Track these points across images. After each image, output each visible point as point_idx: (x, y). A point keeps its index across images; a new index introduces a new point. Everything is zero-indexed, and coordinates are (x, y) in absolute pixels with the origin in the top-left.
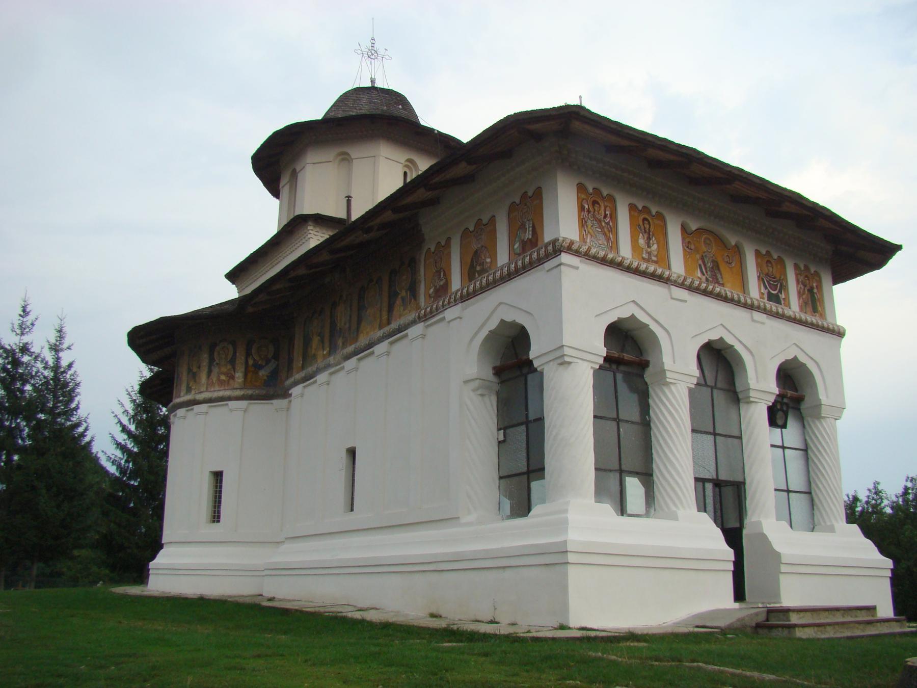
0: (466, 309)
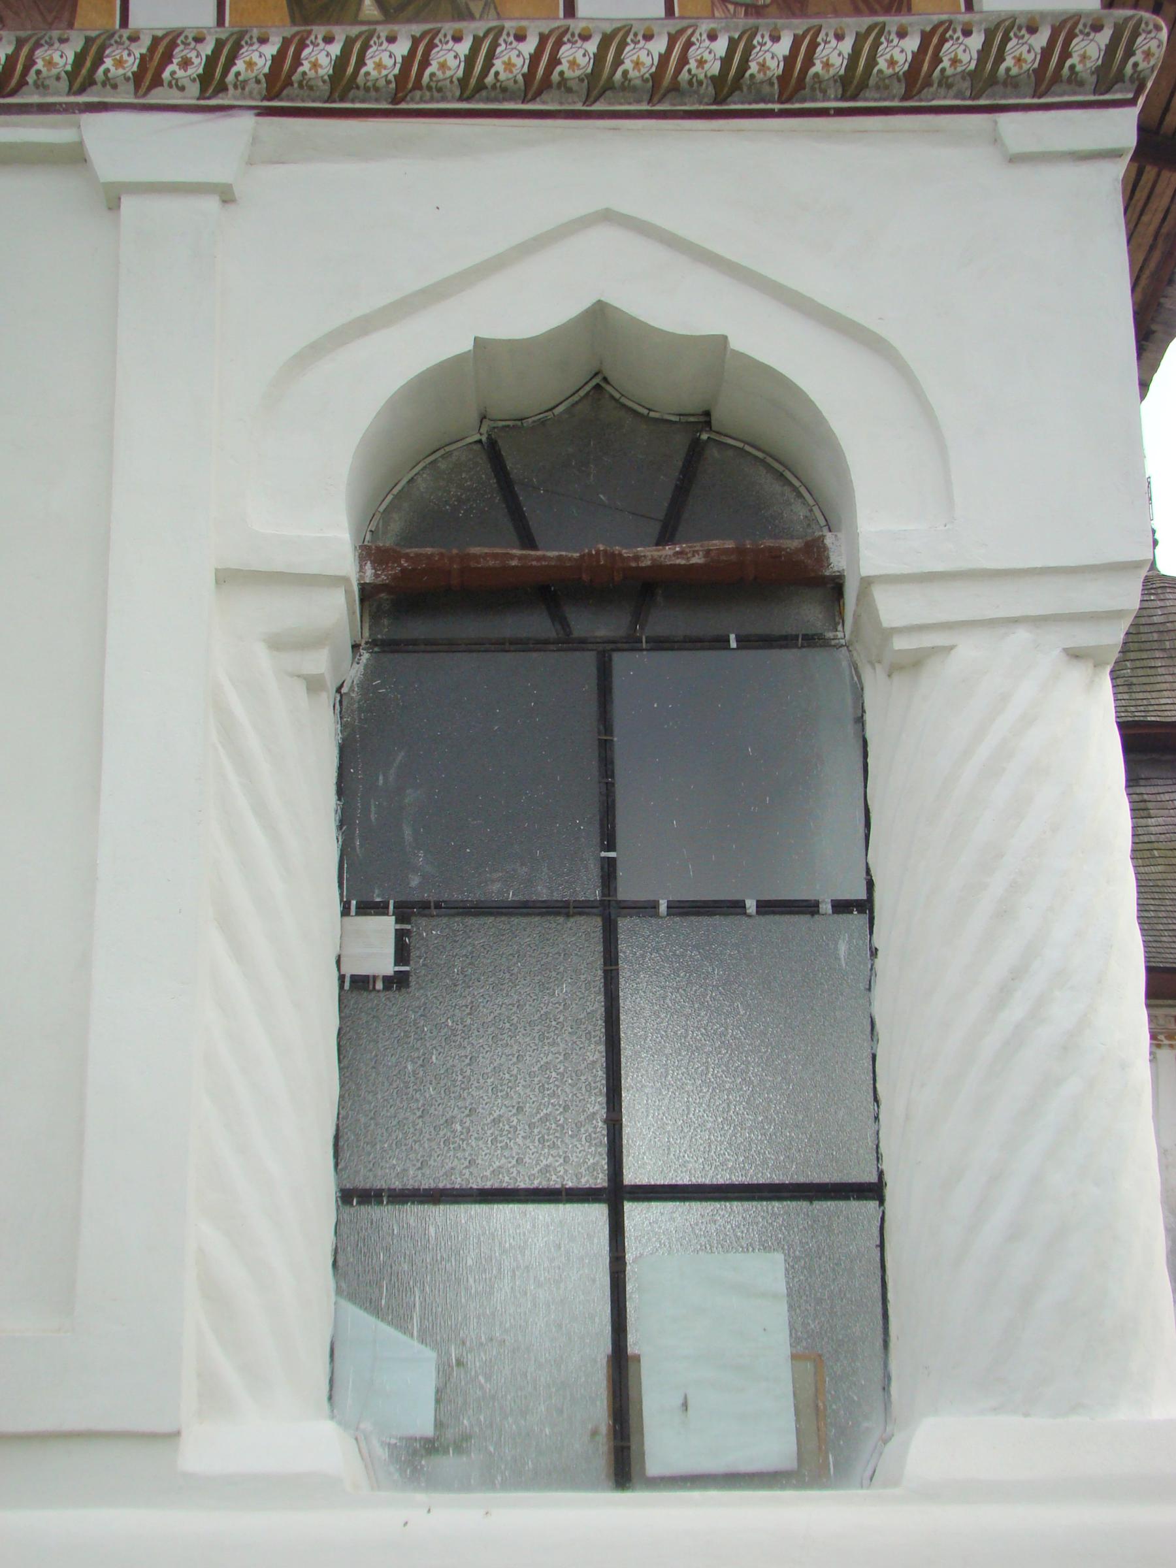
0: (278, 160)
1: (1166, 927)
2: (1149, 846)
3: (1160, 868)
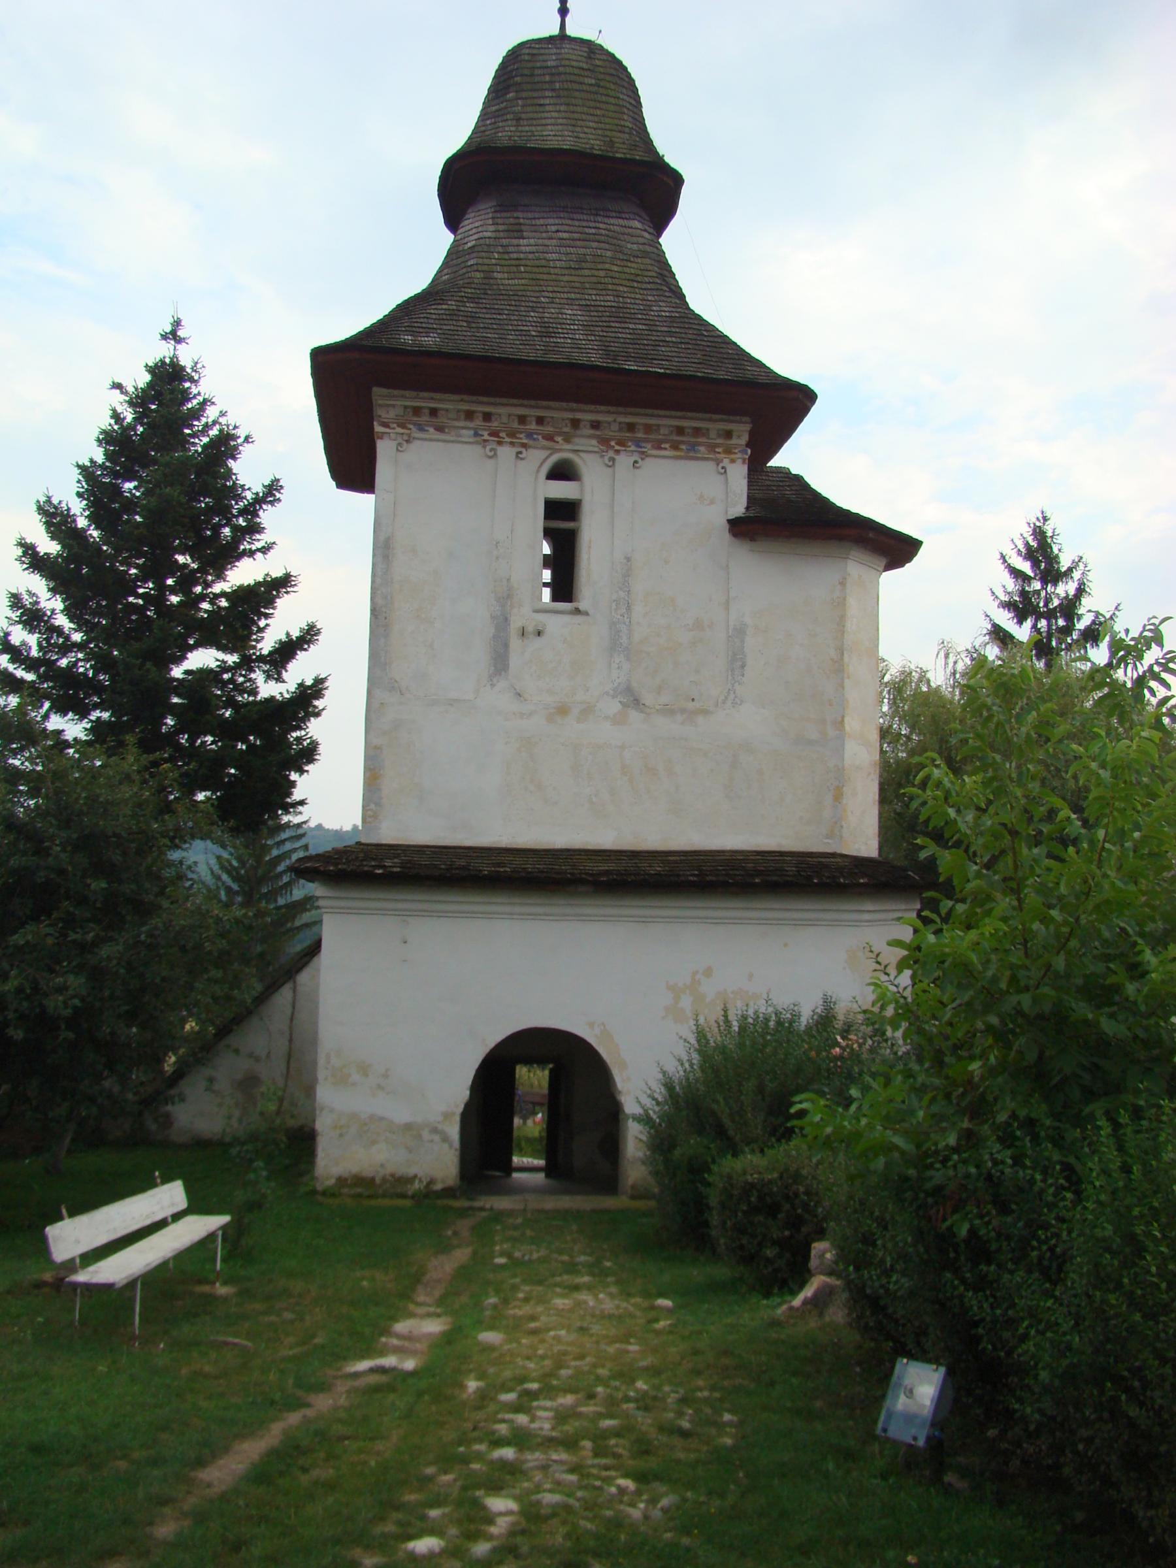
2: (517, 262)
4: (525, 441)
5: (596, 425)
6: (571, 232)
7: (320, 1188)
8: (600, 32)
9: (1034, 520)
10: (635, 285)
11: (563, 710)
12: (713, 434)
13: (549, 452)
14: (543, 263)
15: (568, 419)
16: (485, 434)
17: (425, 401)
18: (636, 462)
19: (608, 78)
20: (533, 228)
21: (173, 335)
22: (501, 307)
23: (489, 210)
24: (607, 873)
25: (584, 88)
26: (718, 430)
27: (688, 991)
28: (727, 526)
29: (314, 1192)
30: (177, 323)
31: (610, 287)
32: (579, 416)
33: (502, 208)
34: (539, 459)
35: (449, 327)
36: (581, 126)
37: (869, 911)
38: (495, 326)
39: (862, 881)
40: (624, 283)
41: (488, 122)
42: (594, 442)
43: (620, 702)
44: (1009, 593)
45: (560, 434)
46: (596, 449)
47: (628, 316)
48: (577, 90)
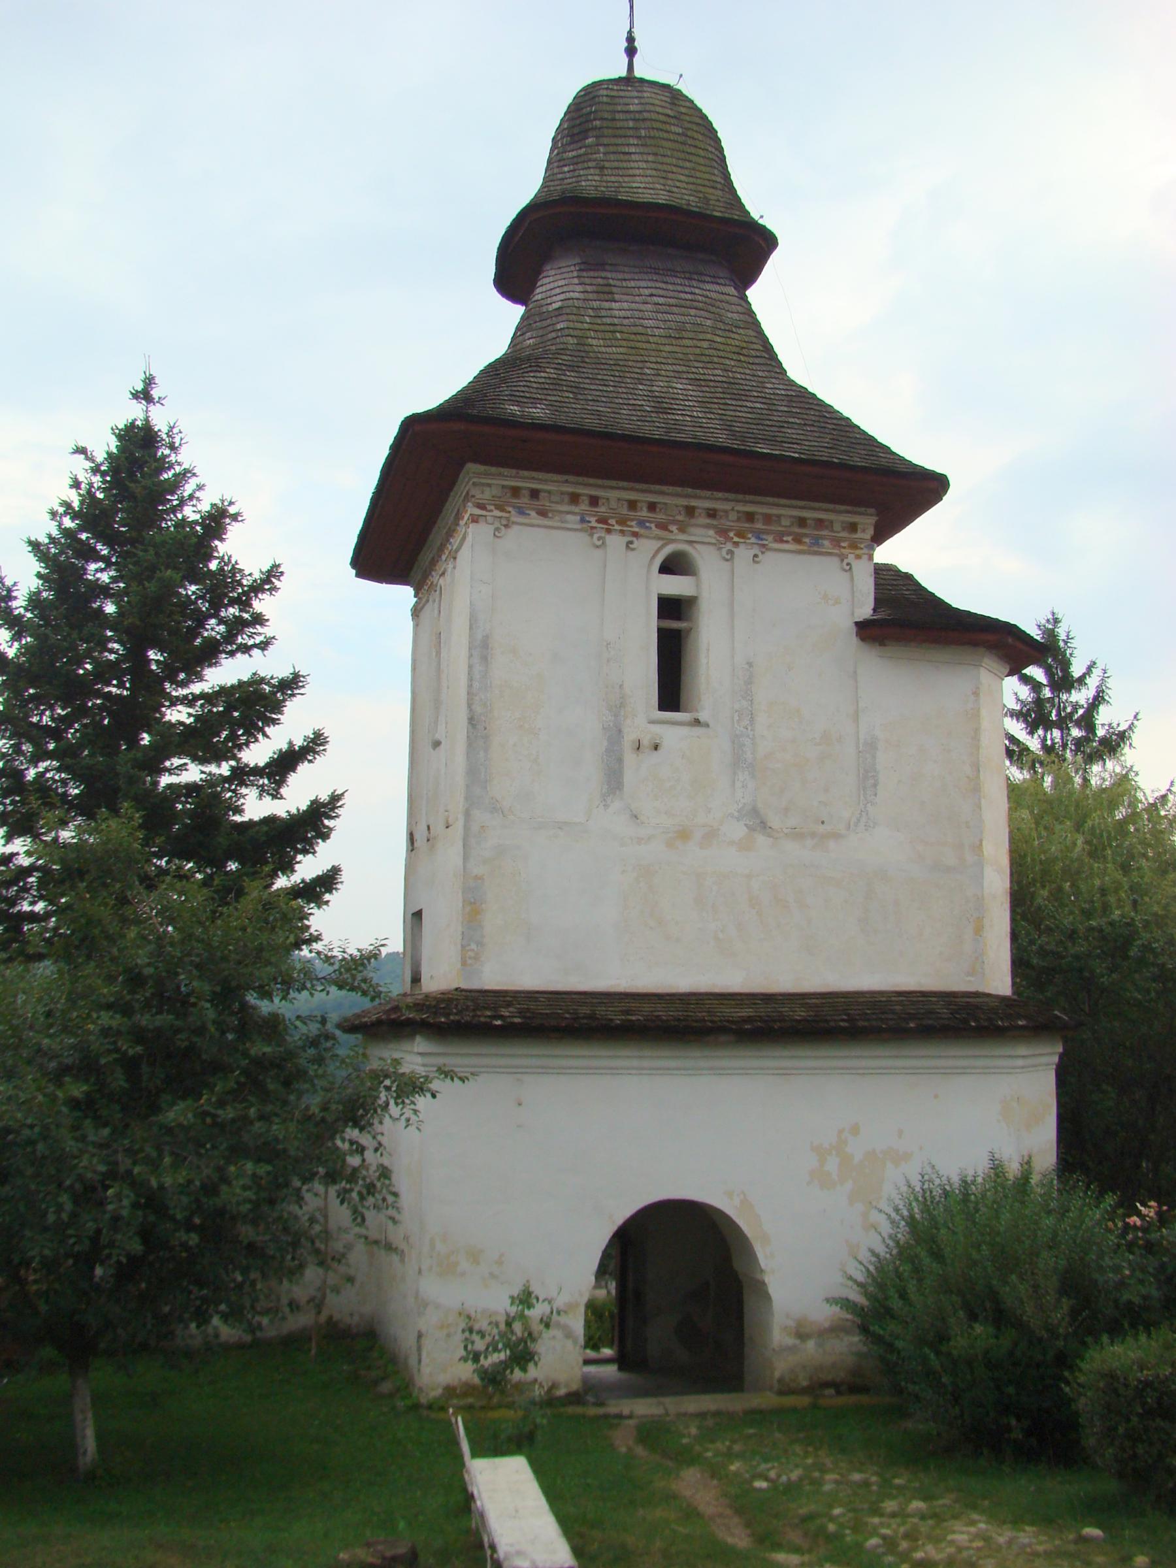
1: (626, 402)
2: (612, 328)
3: (621, 350)
4: (636, 530)
5: (712, 514)
6: (666, 297)
7: (423, 1400)
8: (681, 76)
9: (1043, 622)
10: (742, 358)
11: (684, 835)
12: (837, 527)
13: (660, 543)
14: (641, 330)
15: (682, 506)
16: (593, 519)
17: (526, 481)
18: (756, 556)
19: (695, 127)
20: (624, 290)
21: (145, 395)
22: (605, 378)
23: (572, 268)
24: (749, 1020)
25: (672, 137)
26: (843, 522)
27: (834, 1152)
28: (854, 630)
29: (416, 1406)
30: (149, 382)
31: (716, 360)
32: (694, 503)
33: (587, 266)
34: (651, 550)
35: (553, 398)
36: (672, 180)
37: (1023, 1057)
38: (604, 399)
39: (1020, 1023)
40: (730, 356)
41: (566, 169)
42: (711, 532)
43: (746, 825)
44: (1022, 702)
45: (674, 522)
46: (714, 541)
47: (743, 393)
48: (664, 139)
